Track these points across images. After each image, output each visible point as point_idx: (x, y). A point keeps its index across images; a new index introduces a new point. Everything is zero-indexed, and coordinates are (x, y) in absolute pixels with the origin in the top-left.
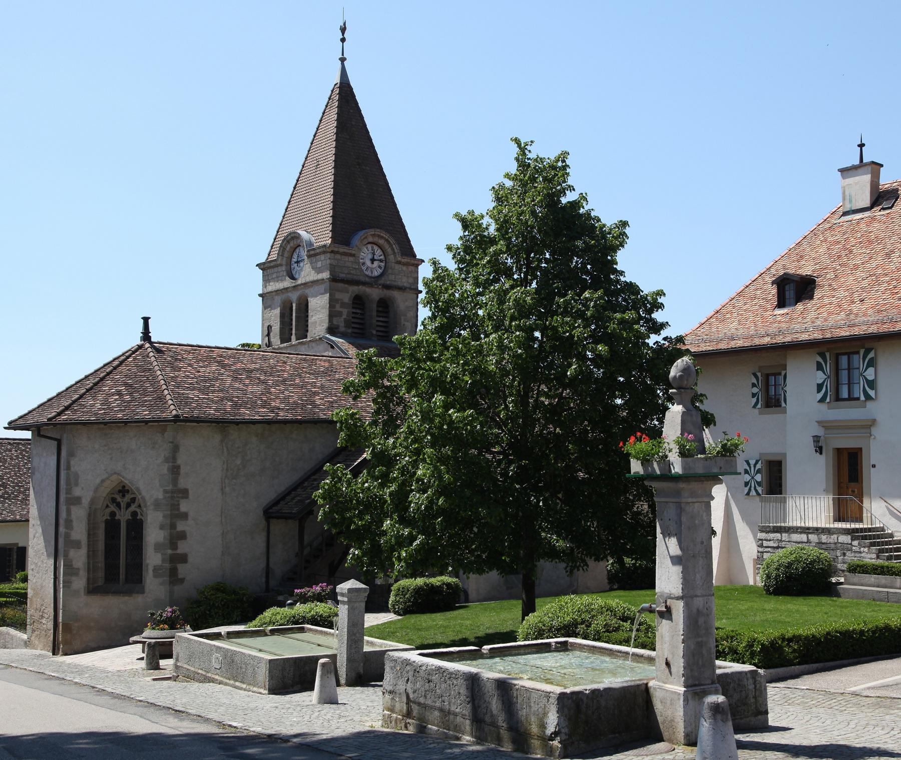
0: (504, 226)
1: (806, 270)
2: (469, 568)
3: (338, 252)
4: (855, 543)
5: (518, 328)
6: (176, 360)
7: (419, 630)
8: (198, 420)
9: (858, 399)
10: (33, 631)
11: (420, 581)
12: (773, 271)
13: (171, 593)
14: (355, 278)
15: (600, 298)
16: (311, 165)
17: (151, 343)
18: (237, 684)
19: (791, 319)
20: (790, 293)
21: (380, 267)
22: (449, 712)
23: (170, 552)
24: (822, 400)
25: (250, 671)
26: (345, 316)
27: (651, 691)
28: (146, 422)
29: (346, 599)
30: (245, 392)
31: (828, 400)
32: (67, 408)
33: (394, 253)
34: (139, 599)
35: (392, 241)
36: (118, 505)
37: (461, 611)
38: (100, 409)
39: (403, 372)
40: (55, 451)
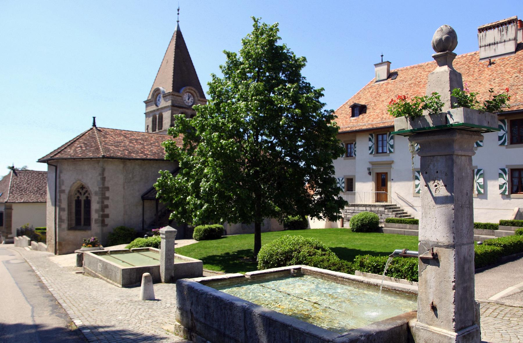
0: (248, 55)
1: (363, 103)
2: (230, 220)
4: (386, 211)
5: (256, 100)
6: (106, 134)
7: (206, 248)
8: (113, 158)
9: (386, 153)
10: (49, 245)
11: (206, 226)
12: (349, 103)
13: (102, 230)
14: (182, 106)
15: (296, 87)
16: (165, 62)
17: (96, 128)
18: (108, 280)
19: (358, 122)
20: (357, 111)
21: (191, 102)
22: (224, 335)
23: (101, 213)
24: (371, 153)
25: (114, 274)
27: (413, 330)
28: (91, 158)
29: (164, 236)
30: (134, 147)
31: (374, 153)
33: (197, 97)
34: (89, 232)
35: (196, 92)
36: (81, 193)
37: (224, 239)
39: (198, 123)
40: (55, 171)
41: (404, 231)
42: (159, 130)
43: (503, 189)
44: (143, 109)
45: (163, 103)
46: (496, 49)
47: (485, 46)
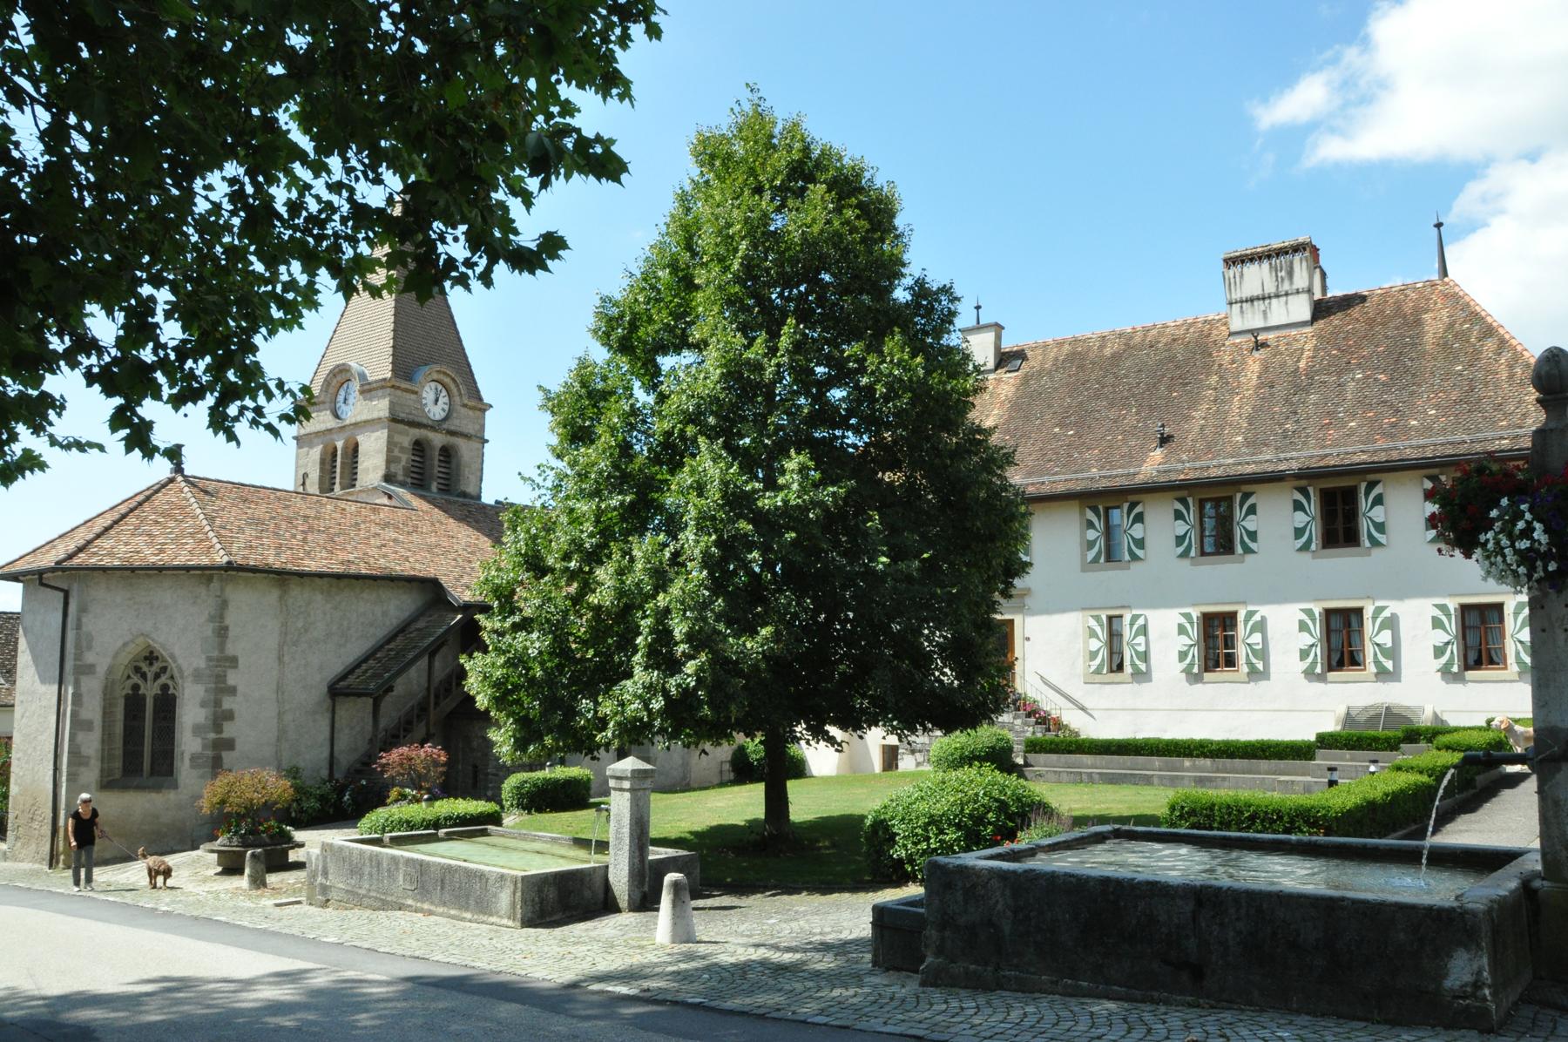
3: (398, 388)
14: (416, 419)
23: (212, 736)
24: (1185, 554)
26: (403, 463)
32: (80, 550)
33: (460, 395)
34: (172, 796)
36: (144, 676)
42: (342, 489)
43: (1310, 659)
45: (357, 409)
47: (1242, 302)
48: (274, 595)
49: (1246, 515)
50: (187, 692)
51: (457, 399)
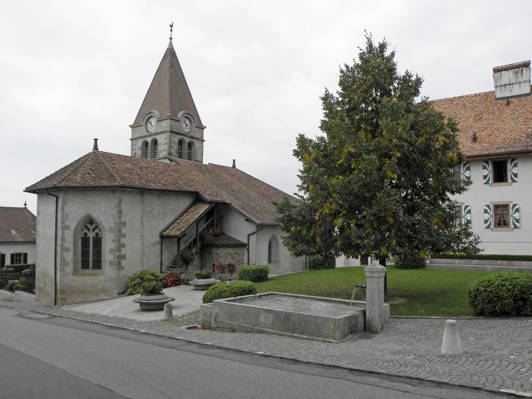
14: (180, 132)
21: (189, 128)
26: (175, 148)
36: (89, 230)
38: (80, 181)
40: (55, 202)
41: (456, 266)
44: (129, 133)
46: (512, 90)
47: (501, 86)
48: (139, 197)
49: (513, 167)
50: (107, 237)
51: (194, 124)
